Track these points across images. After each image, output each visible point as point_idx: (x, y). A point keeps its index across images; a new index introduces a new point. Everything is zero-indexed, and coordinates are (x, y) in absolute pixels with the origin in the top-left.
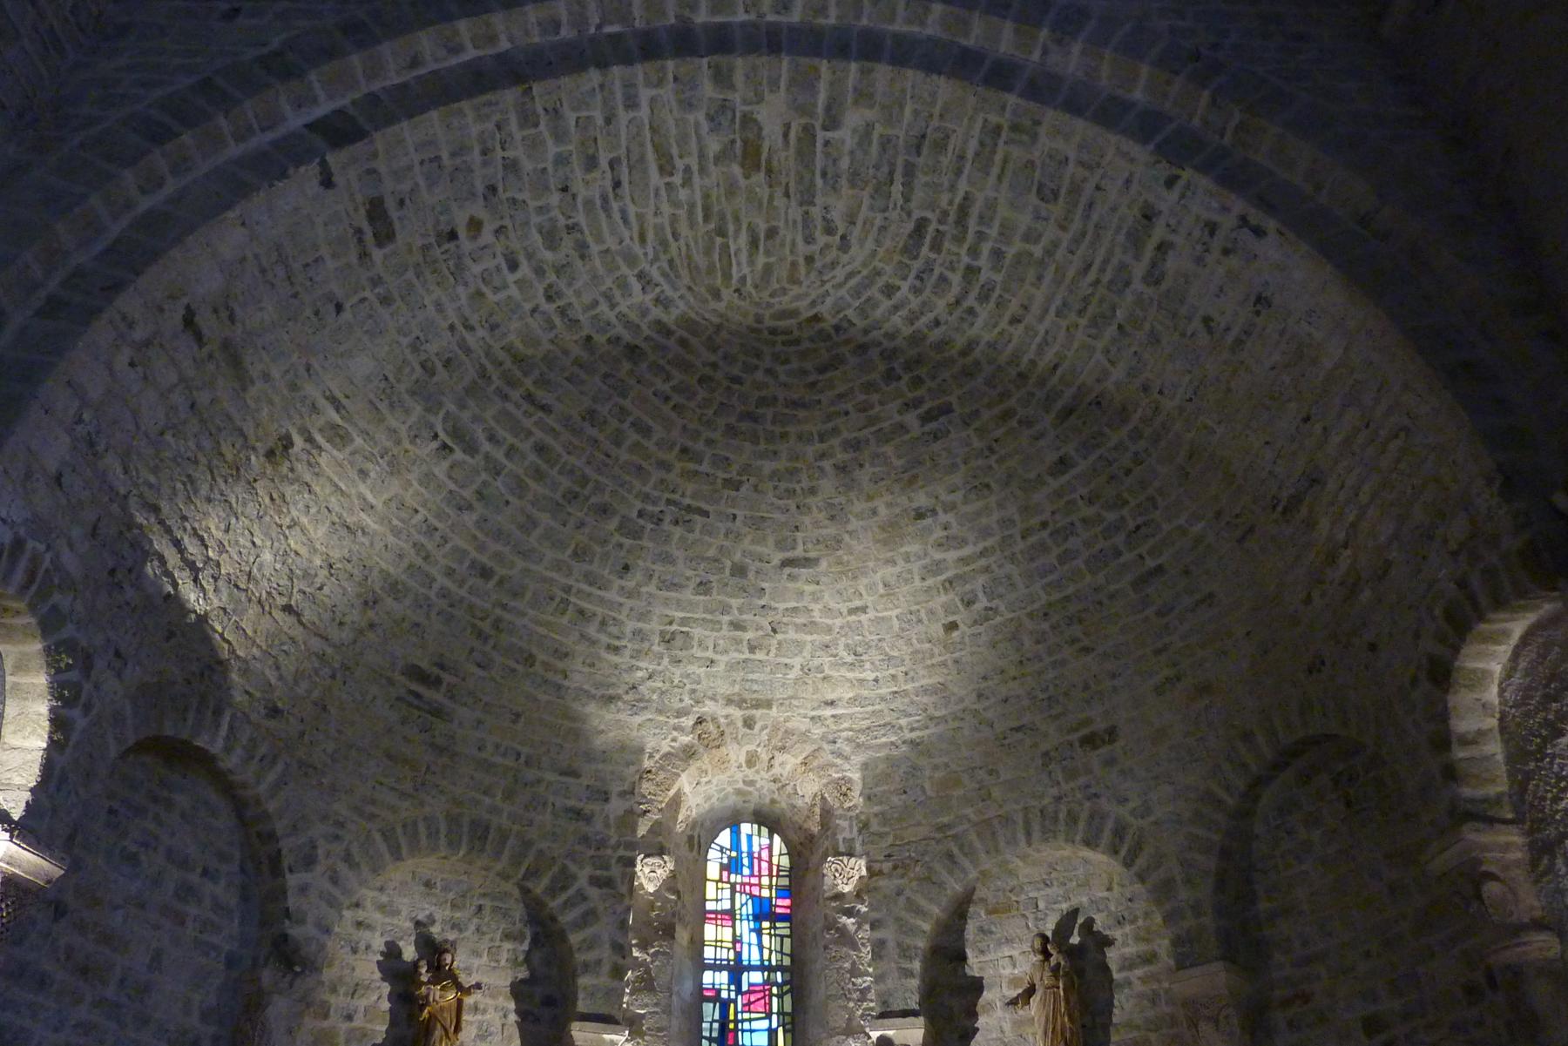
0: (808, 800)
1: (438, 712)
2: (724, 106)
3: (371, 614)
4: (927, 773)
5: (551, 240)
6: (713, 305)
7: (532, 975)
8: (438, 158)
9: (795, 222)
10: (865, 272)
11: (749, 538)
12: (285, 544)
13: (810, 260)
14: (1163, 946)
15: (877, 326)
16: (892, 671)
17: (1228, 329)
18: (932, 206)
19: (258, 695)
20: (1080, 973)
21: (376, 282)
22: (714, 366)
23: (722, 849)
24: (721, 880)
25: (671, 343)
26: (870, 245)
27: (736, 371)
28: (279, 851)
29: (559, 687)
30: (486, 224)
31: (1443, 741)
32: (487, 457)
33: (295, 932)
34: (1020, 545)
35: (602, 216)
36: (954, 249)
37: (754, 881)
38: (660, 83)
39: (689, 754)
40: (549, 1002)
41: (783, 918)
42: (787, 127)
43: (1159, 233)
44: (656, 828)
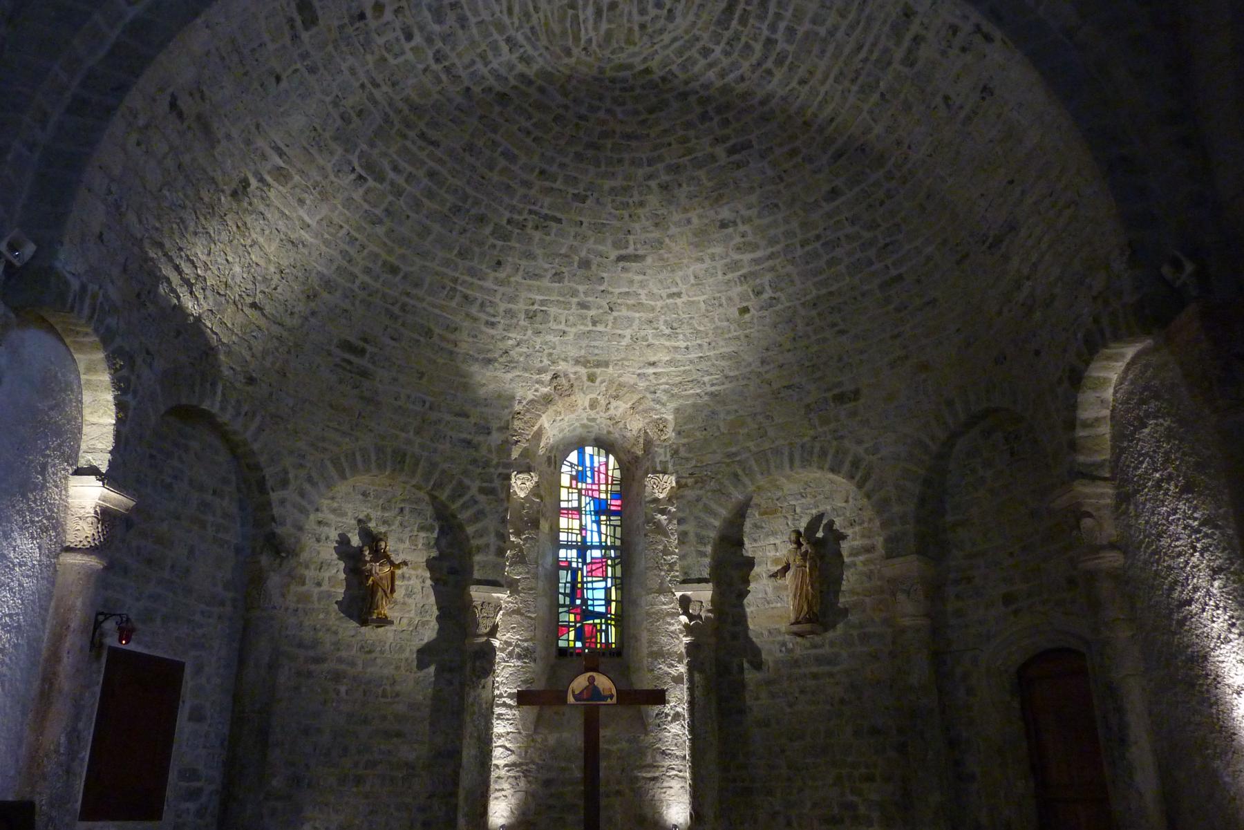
0: (634, 433)
1: (364, 374)
3: (313, 304)
4: (722, 416)
6: (566, 60)
7: (441, 554)
10: (687, 37)
11: (592, 239)
12: (250, 260)
13: (643, 27)
14: (879, 541)
15: (696, 78)
16: (699, 342)
17: (961, 107)
19: (239, 369)
20: (822, 557)
21: (304, 56)
22: (566, 107)
23: (572, 465)
24: (571, 487)
25: (532, 90)
26: (691, 17)
27: (583, 111)
28: (264, 477)
29: (451, 353)
31: (1071, 424)
32: (392, 184)
33: (279, 530)
34: (799, 252)
36: (757, 25)
37: (595, 487)
39: (547, 400)
40: (453, 571)
41: (615, 513)
43: (915, 28)
44: (525, 453)
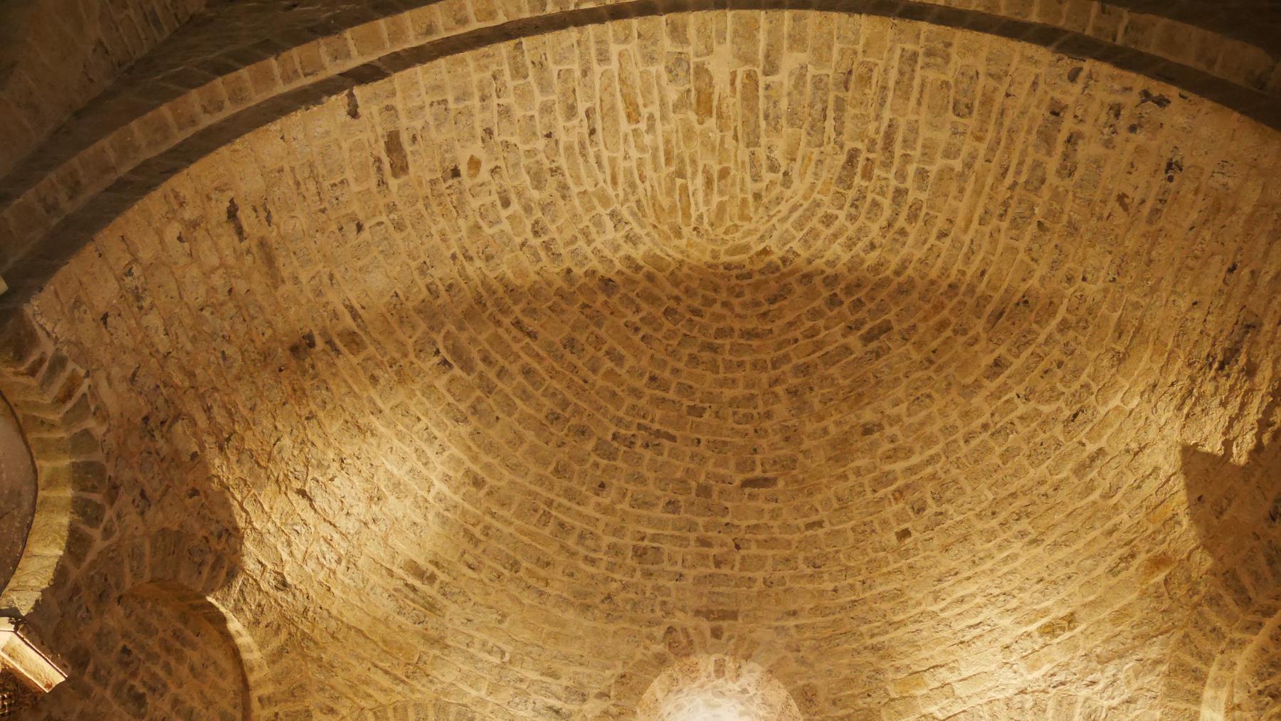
1: (431, 607)
2: (680, 59)
3: (375, 508)
5: (538, 182)
6: (676, 242)
8: (445, 101)
9: (743, 163)
10: (806, 204)
11: (712, 461)
13: (757, 196)
16: (850, 581)
17: (1143, 202)
18: (861, 136)
22: (677, 299)
26: (809, 178)
27: (697, 304)
30: (483, 164)
32: (481, 376)
35: (581, 160)
36: (884, 175)
38: (626, 40)
42: (734, 74)
43: (1068, 125)
